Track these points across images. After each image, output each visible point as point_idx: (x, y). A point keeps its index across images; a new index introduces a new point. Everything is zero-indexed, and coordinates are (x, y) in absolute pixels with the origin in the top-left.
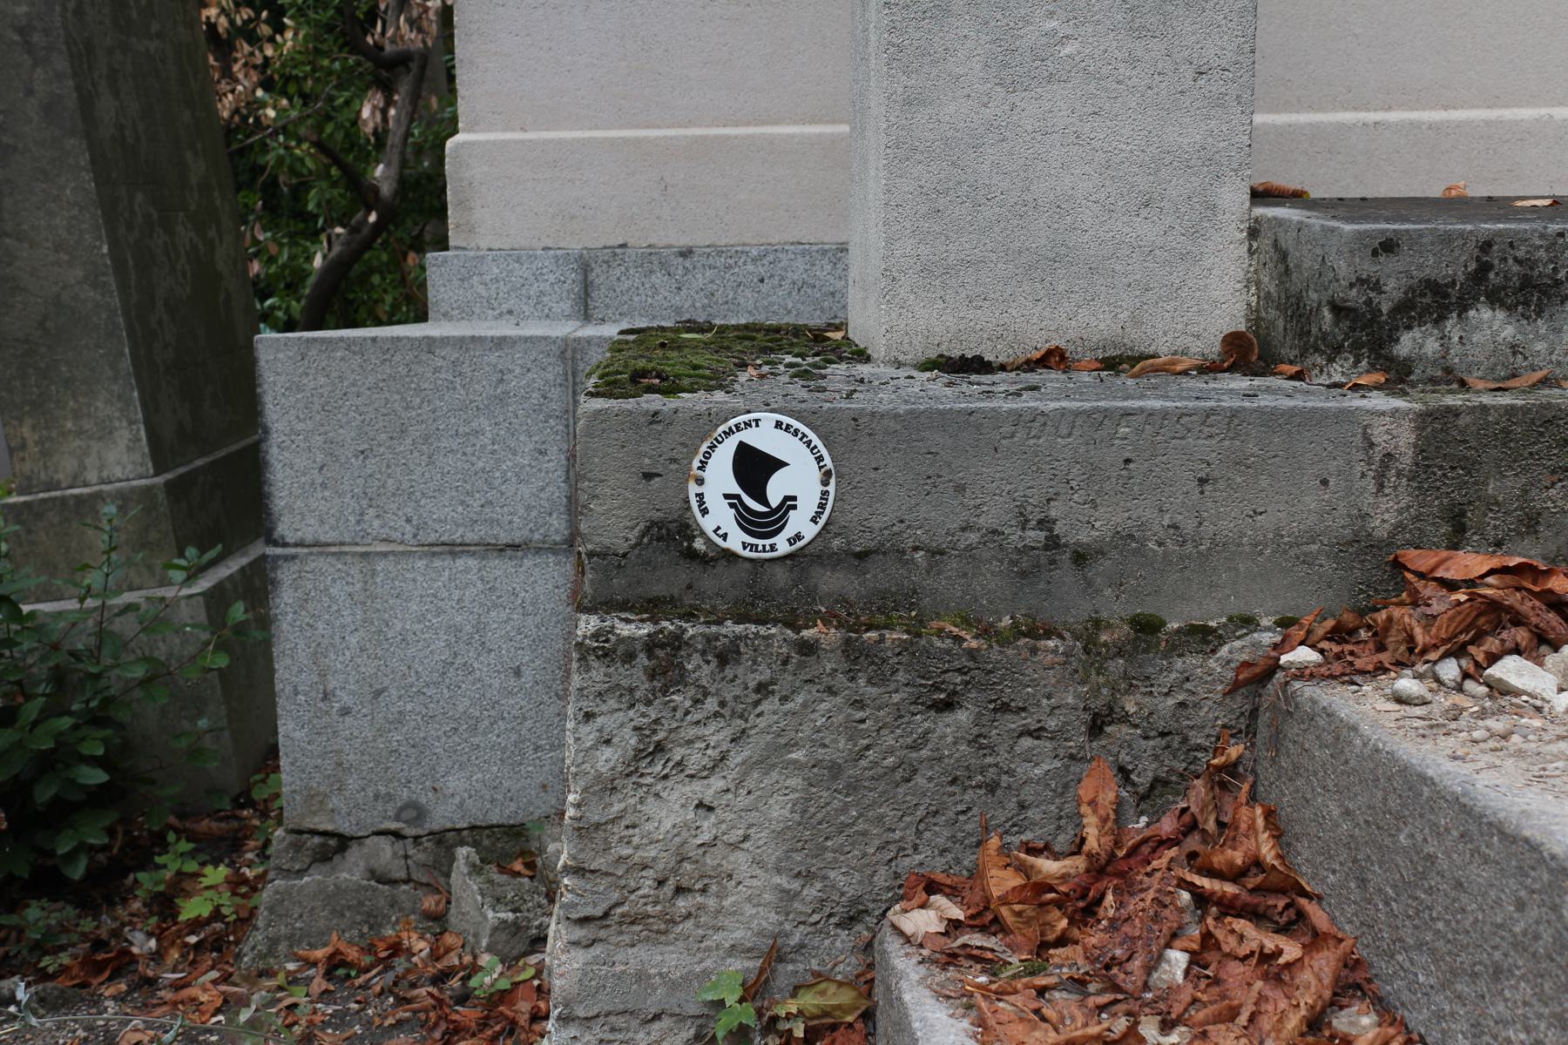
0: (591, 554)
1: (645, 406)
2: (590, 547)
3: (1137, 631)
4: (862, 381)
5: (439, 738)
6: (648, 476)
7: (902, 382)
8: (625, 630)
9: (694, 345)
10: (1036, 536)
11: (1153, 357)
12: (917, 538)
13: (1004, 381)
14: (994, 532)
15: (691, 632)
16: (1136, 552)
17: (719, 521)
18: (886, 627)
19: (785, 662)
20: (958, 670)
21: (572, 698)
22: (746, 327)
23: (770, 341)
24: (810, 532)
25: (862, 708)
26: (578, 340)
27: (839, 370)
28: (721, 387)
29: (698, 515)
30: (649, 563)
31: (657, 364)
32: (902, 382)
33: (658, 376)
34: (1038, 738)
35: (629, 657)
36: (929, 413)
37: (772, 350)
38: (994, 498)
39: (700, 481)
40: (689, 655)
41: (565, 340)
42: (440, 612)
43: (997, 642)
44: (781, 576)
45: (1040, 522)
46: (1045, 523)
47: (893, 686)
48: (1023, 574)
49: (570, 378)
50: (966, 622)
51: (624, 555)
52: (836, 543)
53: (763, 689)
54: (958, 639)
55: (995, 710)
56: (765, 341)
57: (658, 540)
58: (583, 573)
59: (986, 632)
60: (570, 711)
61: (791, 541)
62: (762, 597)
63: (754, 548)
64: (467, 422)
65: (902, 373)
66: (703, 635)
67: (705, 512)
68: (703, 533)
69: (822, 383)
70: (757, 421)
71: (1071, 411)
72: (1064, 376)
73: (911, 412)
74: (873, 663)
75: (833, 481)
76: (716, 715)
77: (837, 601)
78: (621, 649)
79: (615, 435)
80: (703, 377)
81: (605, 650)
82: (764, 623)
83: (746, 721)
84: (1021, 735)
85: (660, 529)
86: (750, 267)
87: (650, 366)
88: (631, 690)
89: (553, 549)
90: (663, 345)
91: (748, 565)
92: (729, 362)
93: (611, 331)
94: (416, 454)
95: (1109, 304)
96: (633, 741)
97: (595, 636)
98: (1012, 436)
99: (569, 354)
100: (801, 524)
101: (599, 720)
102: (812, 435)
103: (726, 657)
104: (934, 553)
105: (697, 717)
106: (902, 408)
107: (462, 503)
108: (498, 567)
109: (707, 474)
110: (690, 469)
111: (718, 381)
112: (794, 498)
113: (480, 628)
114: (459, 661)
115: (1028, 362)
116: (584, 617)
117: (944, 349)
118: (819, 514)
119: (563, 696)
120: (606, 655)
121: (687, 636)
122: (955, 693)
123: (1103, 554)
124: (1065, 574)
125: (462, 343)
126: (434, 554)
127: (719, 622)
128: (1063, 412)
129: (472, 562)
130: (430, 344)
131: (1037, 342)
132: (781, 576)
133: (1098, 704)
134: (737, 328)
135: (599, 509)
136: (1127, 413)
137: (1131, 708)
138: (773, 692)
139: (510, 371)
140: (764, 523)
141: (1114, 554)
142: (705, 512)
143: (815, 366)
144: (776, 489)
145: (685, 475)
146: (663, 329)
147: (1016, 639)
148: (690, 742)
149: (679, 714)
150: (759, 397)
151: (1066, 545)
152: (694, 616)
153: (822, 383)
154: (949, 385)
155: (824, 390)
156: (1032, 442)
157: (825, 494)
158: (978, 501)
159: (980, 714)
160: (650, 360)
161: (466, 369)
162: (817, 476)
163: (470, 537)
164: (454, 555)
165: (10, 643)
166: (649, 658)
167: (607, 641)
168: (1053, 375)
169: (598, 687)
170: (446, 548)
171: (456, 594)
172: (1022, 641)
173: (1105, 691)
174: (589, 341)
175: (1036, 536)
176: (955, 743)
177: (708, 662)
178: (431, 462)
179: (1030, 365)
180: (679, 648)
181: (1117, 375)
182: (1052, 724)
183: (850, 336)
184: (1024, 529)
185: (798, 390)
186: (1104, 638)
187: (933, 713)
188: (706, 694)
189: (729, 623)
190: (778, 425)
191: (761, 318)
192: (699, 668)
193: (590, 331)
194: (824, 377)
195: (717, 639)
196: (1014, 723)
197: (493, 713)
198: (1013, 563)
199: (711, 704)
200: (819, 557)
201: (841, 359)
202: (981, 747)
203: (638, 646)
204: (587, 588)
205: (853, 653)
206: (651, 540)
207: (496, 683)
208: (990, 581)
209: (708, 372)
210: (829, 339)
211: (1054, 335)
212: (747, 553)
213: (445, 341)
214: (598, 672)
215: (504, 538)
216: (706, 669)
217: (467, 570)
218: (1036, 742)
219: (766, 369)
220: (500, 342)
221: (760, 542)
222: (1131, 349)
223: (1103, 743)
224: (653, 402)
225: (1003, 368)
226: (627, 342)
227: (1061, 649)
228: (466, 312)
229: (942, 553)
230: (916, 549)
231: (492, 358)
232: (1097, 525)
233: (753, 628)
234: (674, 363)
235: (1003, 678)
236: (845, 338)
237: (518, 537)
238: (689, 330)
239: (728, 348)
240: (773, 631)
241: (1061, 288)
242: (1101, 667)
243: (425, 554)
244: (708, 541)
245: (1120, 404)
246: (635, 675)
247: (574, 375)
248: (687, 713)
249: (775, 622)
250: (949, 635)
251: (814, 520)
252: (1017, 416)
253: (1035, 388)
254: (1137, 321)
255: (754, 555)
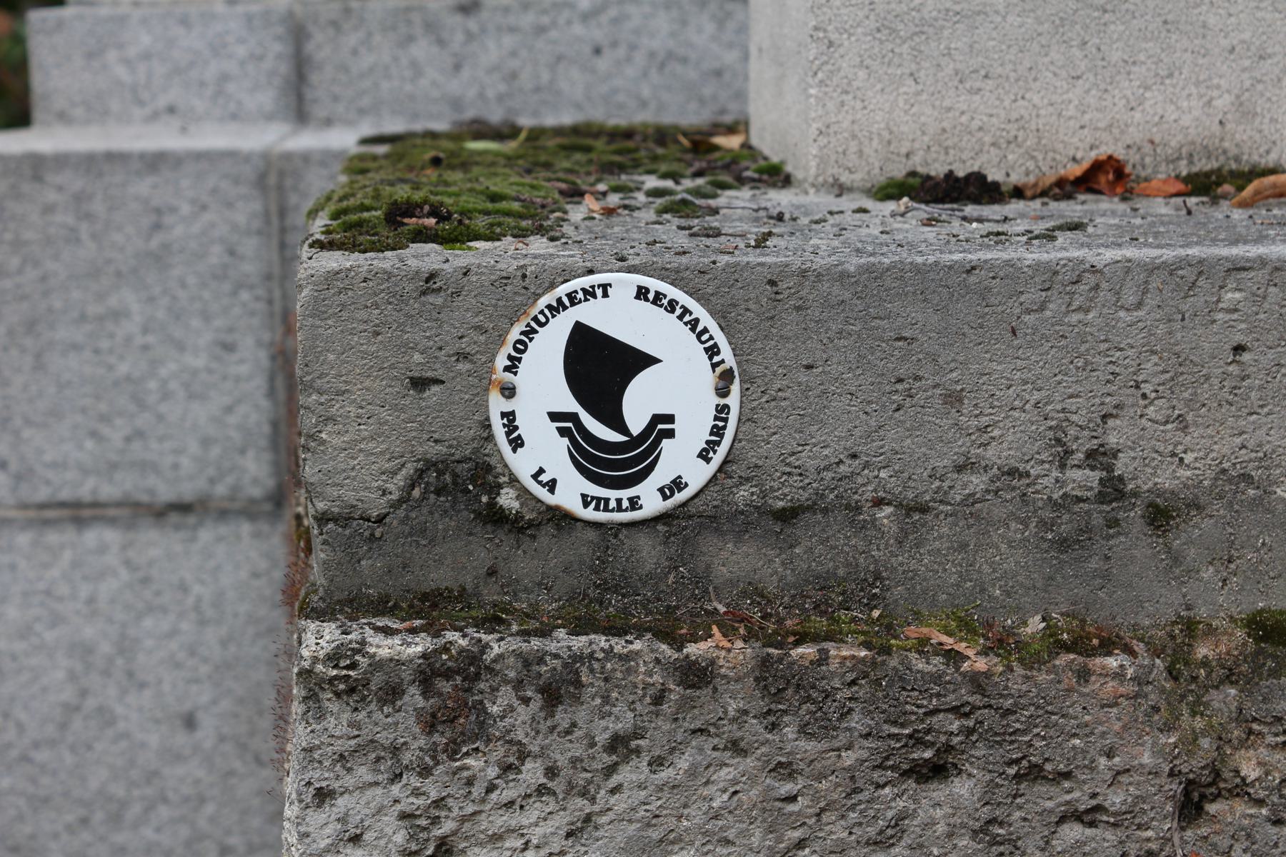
0: (323, 519)
1: (413, 263)
2: (321, 506)
3: (1258, 640)
4: (780, 217)
5: (56, 836)
6: (420, 384)
7: (849, 218)
8: (383, 647)
9: (490, 163)
10: (1084, 479)
11: (1273, 171)
12: (881, 484)
13: (1023, 216)
14: (1012, 472)
15: (496, 649)
16: (1255, 504)
17: (541, 459)
18: (829, 637)
19: (658, 700)
20: (955, 710)
21: (293, 765)
22: (576, 130)
23: (619, 152)
24: (697, 475)
25: (791, 776)
26: (288, 157)
27: (737, 201)
28: (540, 230)
29: (506, 448)
30: (423, 531)
31: (412, 196)
32: (849, 218)
33: (434, 213)
34: (1092, 824)
35: (392, 694)
36: (898, 270)
37: (622, 168)
38: (1011, 415)
39: (509, 392)
40: (494, 690)
41: (266, 156)
42: (56, 620)
43: (1021, 660)
44: (649, 552)
45: (1091, 454)
46: (1098, 457)
47: (843, 739)
48: (1063, 544)
49: (275, 220)
50: (966, 627)
51: (380, 520)
52: (743, 494)
53: (621, 746)
54: (954, 657)
55: (1018, 777)
56: (610, 152)
57: (438, 492)
58: (309, 550)
59: (1001, 644)
60: (290, 786)
61: (665, 492)
62: (616, 589)
63: (602, 504)
64: (101, 297)
65: (848, 203)
66: (518, 654)
67: (517, 443)
68: (514, 481)
69: (713, 222)
70: (605, 287)
71: (1142, 265)
72: (1122, 207)
73: (869, 269)
74: (808, 699)
75: (735, 388)
76: (541, 790)
77: (744, 594)
78: (377, 680)
79: (362, 314)
80: (508, 213)
81: (350, 682)
82: (620, 632)
83: (593, 800)
84: (1062, 820)
85: (440, 473)
86: (578, 29)
87: (418, 196)
88: (395, 750)
89: (249, 511)
90: (436, 162)
91: (591, 534)
92: (549, 189)
93: (345, 139)
94: (14, 352)
95: (1198, 84)
96: (400, 838)
97: (333, 658)
98: (1042, 308)
99: (272, 180)
100: (683, 462)
101: (341, 802)
102: (698, 311)
103: (556, 692)
104: (910, 510)
105: (508, 794)
106: (853, 264)
107: (94, 434)
108: (155, 543)
109: (520, 380)
110: (492, 371)
111: (534, 220)
112: (670, 419)
113: (126, 647)
114: (91, 703)
115: (1061, 183)
116: (312, 626)
117: (918, 163)
118: (712, 446)
119: (279, 763)
120: (351, 691)
121: (489, 657)
122: (949, 748)
123: (1199, 508)
124: (1135, 542)
125: (91, 163)
126: (46, 523)
127: (544, 633)
128: (1128, 267)
129: (111, 536)
130: (37, 165)
131: (1075, 149)
132: (649, 552)
133: (1193, 765)
134: (558, 131)
135: (337, 441)
136: (1238, 267)
137: (1250, 771)
138: (637, 751)
139: (173, 210)
140: (618, 460)
141: (1218, 509)
142: (517, 443)
143: (697, 192)
144: (640, 401)
145: (483, 382)
146: (433, 135)
147: (1053, 655)
148: (497, 838)
149: (477, 791)
150: (608, 247)
151: (1135, 494)
152: (500, 621)
153: (713, 222)
154: (929, 222)
155: (717, 234)
156: (1075, 318)
157: (722, 410)
158: (985, 420)
159: (992, 786)
160: (417, 187)
161: (98, 207)
162: (709, 379)
163: (108, 491)
164: (80, 523)
165: (225, 850)
166: (425, 694)
167: (353, 666)
168: (1106, 204)
169: (340, 746)
170: (65, 513)
171: (85, 590)
172: (1063, 659)
173: (1205, 743)
174: (306, 158)
175: (1084, 479)
176: (950, 835)
177: (526, 701)
178: (39, 365)
179: (1065, 188)
180: (477, 676)
181: (1215, 200)
182: (1115, 799)
183: (755, 141)
184: (1063, 466)
185: (671, 233)
186: (1202, 651)
187: (911, 784)
188: (523, 756)
189: (561, 633)
190: (642, 293)
191: (598, 114)
192: (512, 711)
193: (307, 140)
194: (715, 211)
195: (541, 661)
196: (1050, 798)
197: (149, 791)
198: (1045, 525)
199: (532, 773)
200: (713, 518)
201: (741, 181)
202: (995, 841)
203: (407, 675)
204: (317, 575)
205: (775, 683)
206: (426, 491)
207: (153, 740)
208: (1007, 557)
209: (516, 206)
210: (716, 148)
211: (1105, 136)
212: (590, 514)
213: (62, 161)
214: (338, 719)
215: (166, 494)
216: (523, 713)
217: (102, 549)
218: (1089, 832)
219: (614, 199)
220: (155, 162)
221: (613, 494)
222: (1237, 159)
223: (1204, 831)
224: (425, 257)
225: (1018, 193)
226: (375, 158)
227: (1130, 672)
228: (96, 111)
229: (924, 509)
230: (879, 503)
231: (143, 187)
232: (1188, 458)
233: (602, 641)
234: (457, 191)
235: (1031, 723)
236: (746, 146)
237: (187, 491)
238: (478, 136)
239: (547, 166)
240: (637, 645)
241: (1115, 56)
242: (1198, 702)
243: (29, 524)
244: (524, 493)
245: (1225, 252)
246: (402, 725)
247: (282, 213)
248: (491, 788)
249: (640, 631)
250: (937, 651)
251: (704, 456)
252: (1049, 275)
253: (1076, 227)
254: (1245, 112)
255: (601, 516)
